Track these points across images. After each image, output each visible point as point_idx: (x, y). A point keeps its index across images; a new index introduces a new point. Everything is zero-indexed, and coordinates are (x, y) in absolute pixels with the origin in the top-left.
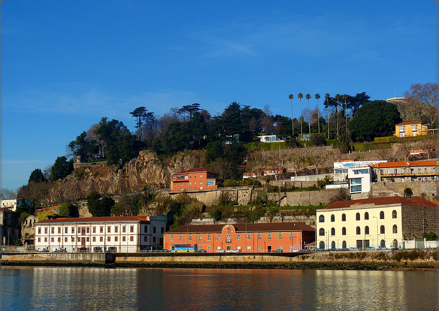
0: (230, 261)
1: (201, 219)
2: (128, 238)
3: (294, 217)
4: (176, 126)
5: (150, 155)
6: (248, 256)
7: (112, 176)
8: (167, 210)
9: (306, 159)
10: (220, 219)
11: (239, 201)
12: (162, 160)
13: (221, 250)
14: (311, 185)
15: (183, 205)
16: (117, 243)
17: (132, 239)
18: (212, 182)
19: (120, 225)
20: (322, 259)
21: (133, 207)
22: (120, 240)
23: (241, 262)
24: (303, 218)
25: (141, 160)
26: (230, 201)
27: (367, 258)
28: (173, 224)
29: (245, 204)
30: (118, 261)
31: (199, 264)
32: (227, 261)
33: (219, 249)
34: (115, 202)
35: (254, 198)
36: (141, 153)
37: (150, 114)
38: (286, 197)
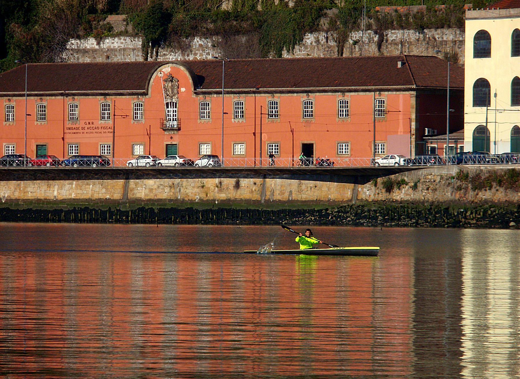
0: (159, 197)
1: (99, 39)
3: (421, 36)
6: (217, 180)
10: (165, 41)
13: (144, 157)
20: (437, 193)
23: (192, 202)
24: (451, 37)
32: (147, 198)
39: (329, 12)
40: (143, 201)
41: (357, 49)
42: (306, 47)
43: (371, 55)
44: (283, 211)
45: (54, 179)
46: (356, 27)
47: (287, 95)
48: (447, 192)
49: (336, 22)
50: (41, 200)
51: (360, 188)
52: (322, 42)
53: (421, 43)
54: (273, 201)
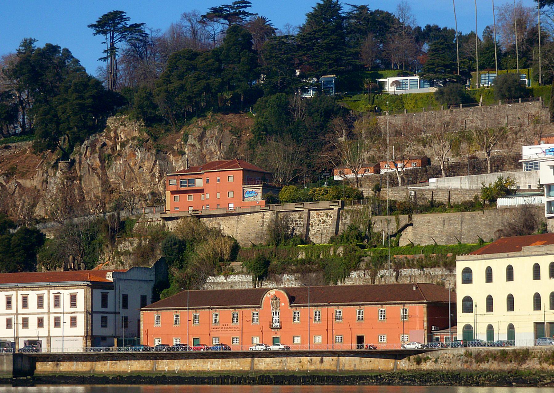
1: (226, 276)
2: (66, 319)
3: (422, 272)
4: (187, 59)
5: (131, 128)
6: (309, 358)
7: (45, 175)
8: (158, 256)
9: (475, 136)
10: (266, 277)
11: (313, 235)
12: (156, 139)
13: (260, 345)
14: (469, 198)
15: (191, 245)
16: (43, 332)
17: (74, 322)
18: (255, 193)
19: (49, 292)
20: (451, 364)
21: (84, 250)
22: (49, 324)
23: (294, 371)
24: (440, 273)
25: (110, 138)
26: (292, 234)
27: (532, 363)
28: (168, 286)
29: (325, 241)
30: (41, 371)
31: (209, 375)
33: (256, 344)
34: (47, 237)
35: (343, 228)
36: (110, 122)
37: (136, 28)
38: (411, 225)
39: (365, 258)
40: (263, 371)
41: (383, 280)
42: (352, 280)
43: (392, 283)
44: (352, 377)
45: (207, 358)
46: (382, 267)
47: (347, 307)
48: (458, 364)
49: (370, 265)
50: (200, 371)
51: (398, 362)
52: (362, 277)
53: (422, 277)
54: (344, 370)
